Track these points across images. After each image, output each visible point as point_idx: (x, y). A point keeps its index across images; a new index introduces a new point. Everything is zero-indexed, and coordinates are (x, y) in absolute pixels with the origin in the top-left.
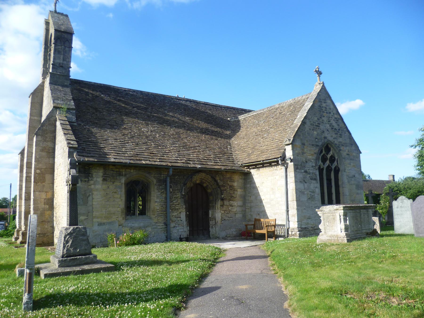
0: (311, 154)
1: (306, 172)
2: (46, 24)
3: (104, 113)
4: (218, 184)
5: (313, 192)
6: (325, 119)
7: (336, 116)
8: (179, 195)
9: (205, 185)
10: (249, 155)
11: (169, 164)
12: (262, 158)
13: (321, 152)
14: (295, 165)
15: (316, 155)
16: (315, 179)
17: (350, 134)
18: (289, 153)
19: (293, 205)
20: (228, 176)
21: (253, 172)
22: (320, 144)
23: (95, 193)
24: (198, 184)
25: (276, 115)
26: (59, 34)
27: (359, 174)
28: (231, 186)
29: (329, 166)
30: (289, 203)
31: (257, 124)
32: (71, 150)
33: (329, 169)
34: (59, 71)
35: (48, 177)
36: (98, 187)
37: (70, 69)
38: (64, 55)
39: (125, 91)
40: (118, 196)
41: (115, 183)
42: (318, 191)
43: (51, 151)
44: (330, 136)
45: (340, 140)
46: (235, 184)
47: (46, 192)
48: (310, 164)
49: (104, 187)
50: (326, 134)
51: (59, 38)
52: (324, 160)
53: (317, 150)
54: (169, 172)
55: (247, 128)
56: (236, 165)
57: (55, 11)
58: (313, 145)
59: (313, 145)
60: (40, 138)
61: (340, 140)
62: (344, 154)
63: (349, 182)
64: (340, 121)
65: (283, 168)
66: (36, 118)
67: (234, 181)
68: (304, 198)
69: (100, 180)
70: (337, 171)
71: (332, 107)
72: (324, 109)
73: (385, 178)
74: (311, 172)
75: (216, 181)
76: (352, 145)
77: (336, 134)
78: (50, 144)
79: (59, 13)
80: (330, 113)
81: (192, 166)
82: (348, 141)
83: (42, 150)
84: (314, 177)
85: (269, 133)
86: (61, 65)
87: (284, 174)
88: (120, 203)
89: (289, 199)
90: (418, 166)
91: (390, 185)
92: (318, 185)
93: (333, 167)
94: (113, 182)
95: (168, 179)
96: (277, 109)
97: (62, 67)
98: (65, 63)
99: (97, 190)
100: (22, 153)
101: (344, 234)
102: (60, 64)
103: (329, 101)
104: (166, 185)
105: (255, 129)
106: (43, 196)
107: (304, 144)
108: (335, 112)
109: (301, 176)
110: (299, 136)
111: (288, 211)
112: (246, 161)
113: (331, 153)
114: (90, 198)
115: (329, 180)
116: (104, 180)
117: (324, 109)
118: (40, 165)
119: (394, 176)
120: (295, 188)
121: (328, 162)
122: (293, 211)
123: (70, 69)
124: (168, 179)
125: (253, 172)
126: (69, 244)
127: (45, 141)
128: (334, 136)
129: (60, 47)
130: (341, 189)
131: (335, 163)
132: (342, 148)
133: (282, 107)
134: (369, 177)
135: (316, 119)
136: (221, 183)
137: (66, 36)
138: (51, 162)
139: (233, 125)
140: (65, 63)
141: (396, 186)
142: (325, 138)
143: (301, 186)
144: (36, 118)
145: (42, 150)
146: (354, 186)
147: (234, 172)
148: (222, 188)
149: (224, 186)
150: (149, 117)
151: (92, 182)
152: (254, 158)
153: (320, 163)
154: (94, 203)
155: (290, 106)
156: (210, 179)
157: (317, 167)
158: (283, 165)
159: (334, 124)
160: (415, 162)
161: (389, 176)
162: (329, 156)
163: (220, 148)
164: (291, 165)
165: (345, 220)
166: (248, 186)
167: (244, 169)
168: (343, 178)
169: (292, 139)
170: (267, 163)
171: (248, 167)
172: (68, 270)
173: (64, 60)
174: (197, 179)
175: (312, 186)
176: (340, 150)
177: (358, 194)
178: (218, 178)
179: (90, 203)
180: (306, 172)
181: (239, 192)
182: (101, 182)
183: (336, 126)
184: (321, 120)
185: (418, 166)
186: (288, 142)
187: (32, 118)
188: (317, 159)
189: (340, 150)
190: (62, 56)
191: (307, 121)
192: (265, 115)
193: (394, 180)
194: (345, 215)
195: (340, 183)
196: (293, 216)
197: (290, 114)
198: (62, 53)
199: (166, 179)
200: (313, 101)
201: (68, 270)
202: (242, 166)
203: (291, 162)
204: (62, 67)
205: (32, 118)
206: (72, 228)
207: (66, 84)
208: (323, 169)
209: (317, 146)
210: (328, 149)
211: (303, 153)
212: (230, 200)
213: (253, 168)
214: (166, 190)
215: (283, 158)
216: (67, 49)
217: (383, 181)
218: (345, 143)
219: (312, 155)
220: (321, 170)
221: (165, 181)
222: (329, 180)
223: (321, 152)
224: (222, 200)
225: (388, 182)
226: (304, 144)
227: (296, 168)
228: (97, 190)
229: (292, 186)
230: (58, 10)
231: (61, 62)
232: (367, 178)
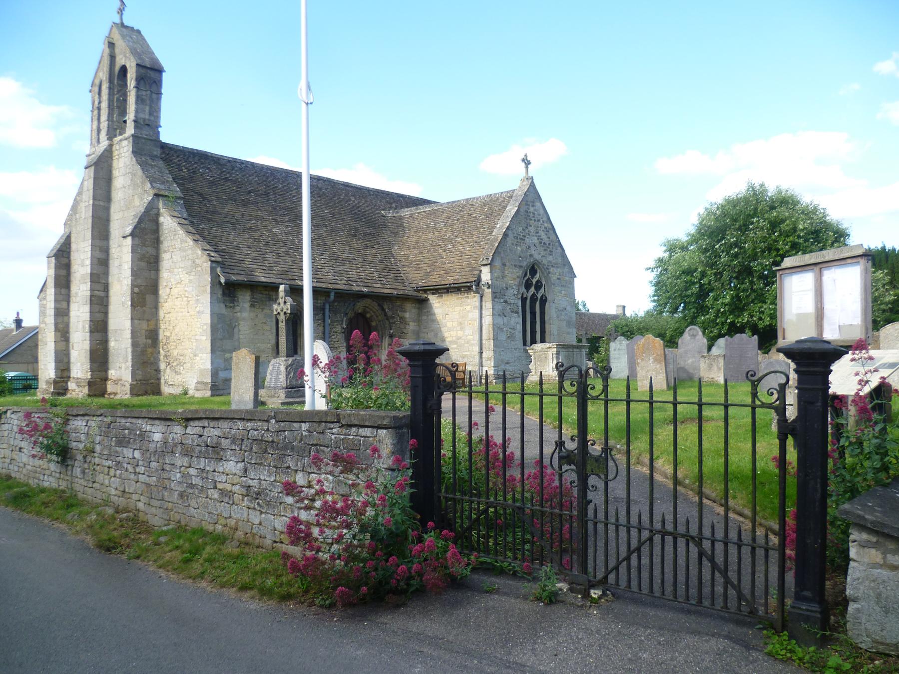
0: (513, 278)
1: (506, 302)
2: (109, 47)
3: (214, 202)
4: (386, 315)
5: (514, 329)
6: (532, 229)
7: (546, 225)
8: (339, 329)
9: (368, 315)
10: (427, 275)
11: (330, 286)
12: (449, 280)
13: (526, 275)
14: (493, 292)
15: (518, 280)
16: (517, 312)
17: (563, 250)
18: (486, 276)
19: (489, 344)
20: (398, 303)
21: (433, 299)
22: (525, 264)
23: (241, 323)
24: (360, 314)
25: (462, 217)
26: (143, 71)
27: (572, 307)
28: (401, 318)
29: (534, 295)
30: (484, 342)
31: (433, 228)
32: (214, 265)
33: (534, 299)
34: (145, 132)
35: (149, 298)
36: (245, 315)
37: (160, 129)
38: (151, 106)
39: (229, 161)
40: (268, 328)
41: (265, 311)
42: (519, 327)
43: (152, 261)
44: (537, 254)
45: (550, 258)
46: (407, 315)
47: (148, 320)
48: (511, 292)
49: (252, 315)
50: (532, 251)
51: (142, 78)
52: (528, 286)
53: (520, 273)
54: (329, 296)
55: (417, 231)
56: (408, 288)
57: (122, 24)
58: (515, 266)
59: (515, 266)
60: (137, 241)
61: (550, 258)
62: (554, 278)
63: (558, 317)
64: (551, 232)
65: (478, 296)
66: (102, 203)
67: (405, 311)
68: (503, 337)
69: (247, 305)
70: (544, 301)
71: (542, 211)
72: (531, 215)
73: (612, 310)
74: (512, 301)
75: (383, 310)
76: (565, 265)
77: (545, 250)
78: (151, 251)
79: (127, 27)
80: (539, 221)
81: (357, 289)
82: (560, 260)
83: (141, 259)
84: (515, 310)
85: (454, 245)
86: (147, 122)
87: (478, 304)
88: (270, 337)
89: (485, 336)
90: (654, 296)
91: (617, 322)
92: (520, 320)
93: (539, 296)
94: (263, 309)
95: (327, 306)
96: (463, 207)
97: (148, 125)
98: (152, 118)
99: (244, 319)
100: (62, 255)
101: (556, 373)
102: (144, 120)
103: (538, 204)
104: (324, 314)
105: (430, 236)
106: (144, 325)
107: (504, 265)
108: (545, 219)
109: (499, 307)
110: (500, 253)
111: (481, 353)
112: (423, 283)
113: (537, 277)
114: (236, 330)
115: (533, 314)
116: (252, 306)
117: (531, 215)
118: (139, 282)
119: (624, 307)
120: (40, 347)
121: (533, 289)
122: (488, 353)
123: (160, 129)
124: (327, 306)
125: (433, 299)
126: (292, 375)
127: (144, 245)
128: (543, 253)
129: (144, 93)
130: (547, 326)
131: (542, 290)
132: (551, 271)
133: (472, 205)
134: (585, 305)
135: (521, 229)
136: (389, 313)
137: (152, 74)
138: (153, 277)
139: (393, 224)
140: (152, 118)
141: (627, 325)
142: (531, 256)
143: (500, 321)
144: (102, 203)
145: (141, 259)
146: (565, 323)
147: (405, 298)
148: (391, 321)
149: (393, 318)
150: (275, 209)
151: (238, 309)
152: (434, 280)
153: (523, 289)
154: (241, 337)
155: (485, 205)
156: (377, 307)
157: (520, 296)
158: (477, 292)
159: (543, 236)
160: (651, 290)
161: (618, 306)
162: (534, 281)
163: (381, 261)
164: (488, 292)
165: (557, 358)
166: (424, 318)
167: (419, 295)
168: (551, 311)
169: (490, 258)
170: (455, 288)
171: (425, 291)
172: (291, 400)
173: (150, 114)
174: (360, 306)
175: (513, 321)
176: (549, 273)
177: (568, 333)
178: (385, 307)
179: (236, 336)
180: (506, 302)
181: (412, 326)
182: (248, 309)
183: (546, 240)
184: (527, 231)
185: (654, 296)
186: (484, 262)
187: (97, 203)
188: (520, 285)
189: (549, 273)
190: (147, 109)
191: (510, 233)
192: (446, 215)
193: (624, 314)
194: (558, 354)
195: (547, 318)
196: (489, 359)
197: (484, 219)
198: (148, 102)
199: (324, 305)
200: (518, 204)
201: (291, 400)
202: (418, 290)
203: (489, 288)
204: (148, 125)
205: (97, 203)
206: (291, 359)
207: (155, 153)
208: (526, 298)
209: (521, 267)
210: (533, 270)
211: (503, 277)
212: (400, 337)
213: (433, 294)
214: (324, 321)
215: (478, 281)
216: (154, 96)
217: (606, 315)
218: (556, 264)
219: (514, 279)
220: (524, 300)
221: (323, 309)
222: (533, 314)
223: (526, 275)
224: (391, 336)
225: (615, 317)
226: (504, 265)
227: (495, 296)
228: (244, 319)
229: (488, 320)
230: (126, 23)
231: (147, 117)
232: (581, 307)
